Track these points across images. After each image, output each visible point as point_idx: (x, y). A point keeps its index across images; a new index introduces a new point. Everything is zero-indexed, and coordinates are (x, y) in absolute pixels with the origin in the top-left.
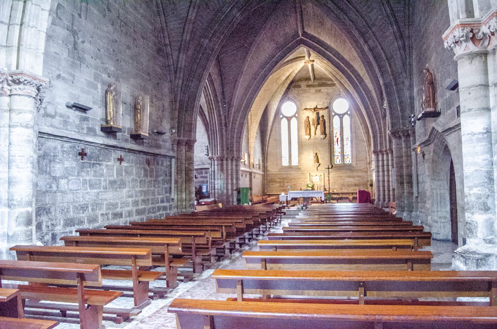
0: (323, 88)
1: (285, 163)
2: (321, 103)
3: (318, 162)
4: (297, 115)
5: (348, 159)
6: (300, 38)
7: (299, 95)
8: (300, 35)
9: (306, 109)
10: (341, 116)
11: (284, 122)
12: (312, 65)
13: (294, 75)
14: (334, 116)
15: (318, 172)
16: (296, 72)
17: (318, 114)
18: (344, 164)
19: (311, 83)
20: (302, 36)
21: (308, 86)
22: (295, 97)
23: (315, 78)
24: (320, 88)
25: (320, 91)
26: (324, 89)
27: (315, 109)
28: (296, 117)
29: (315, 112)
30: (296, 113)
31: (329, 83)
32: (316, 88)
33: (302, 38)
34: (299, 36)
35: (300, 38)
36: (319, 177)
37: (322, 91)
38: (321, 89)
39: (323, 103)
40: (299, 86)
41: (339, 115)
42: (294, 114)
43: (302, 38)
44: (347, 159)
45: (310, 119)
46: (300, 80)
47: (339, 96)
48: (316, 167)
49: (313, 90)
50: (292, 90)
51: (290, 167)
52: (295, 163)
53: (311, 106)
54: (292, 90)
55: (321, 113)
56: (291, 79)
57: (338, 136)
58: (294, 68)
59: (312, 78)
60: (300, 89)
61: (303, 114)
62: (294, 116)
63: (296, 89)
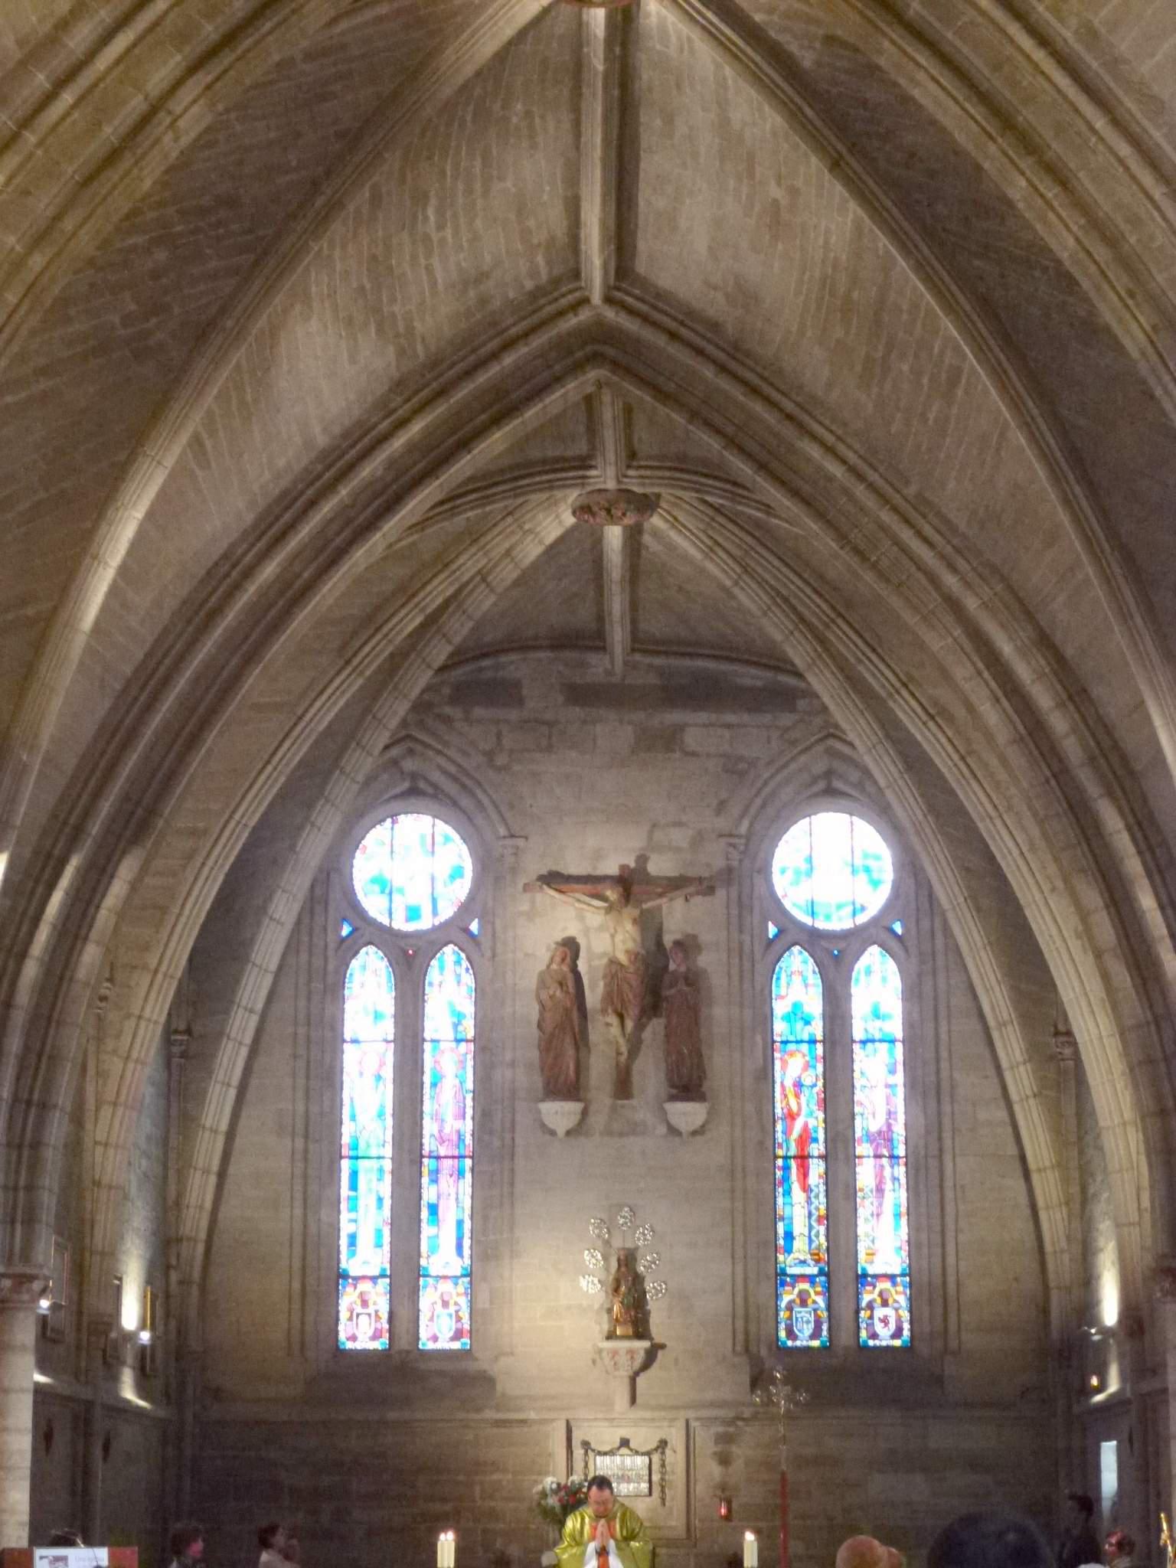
0: (703, 717)
1: (361, 1327)
2: (679, 837)
3: (640, 1331)
4: (475, 931)
5: (889, 1311)
6: (584, 315)
7: (501, 760)
8: (596, 297)
9: (555, 880)
10: (834, 955)
11: (368, 986)
12: (633, 536)
13: (483, 603)
14: (349, 949)
15: (637, 1413)
16: (507, 574)
17: (650, 926)
18: (341, 1157)
19: (598, 668)
20: (608, 300)
21: (581, 695)
22: (463, 780)
23: (639, 643)
24: (673, 717)
25: (670, 741)
26: (701, 730)
27: (629, 885)
28: (469, 944)
29: (631, 912)
30: (466, 909)
31: (751, 677)
32: (640, 716)
33: (610, 314)
34: (586, 301)
35: (584, 315)
36: (641, 1461)
37: (692, 738)
38: (681, 728)
39: (698, 840)
40: (506, 693)
41: (814, 940)
42: (447, 912)
43: (610, 314)
44: (880, 1312)
45: (582, 966)
46: (518, 644)
47: (828, 790)
48: (625, 1373)
49: (614, 731)
50: (447, 720)
51: (401, 1368)
52: (439, 1328)
53: (598, 855)
54: (447, 720)
55: (678, 917)
56: (459, 629)
57: (812, 1117)
58: (498, 545)
59: (618, 636)
60: (513, 715)
61: (531, 916)
62: (453, 932)
63: (479, 712)
